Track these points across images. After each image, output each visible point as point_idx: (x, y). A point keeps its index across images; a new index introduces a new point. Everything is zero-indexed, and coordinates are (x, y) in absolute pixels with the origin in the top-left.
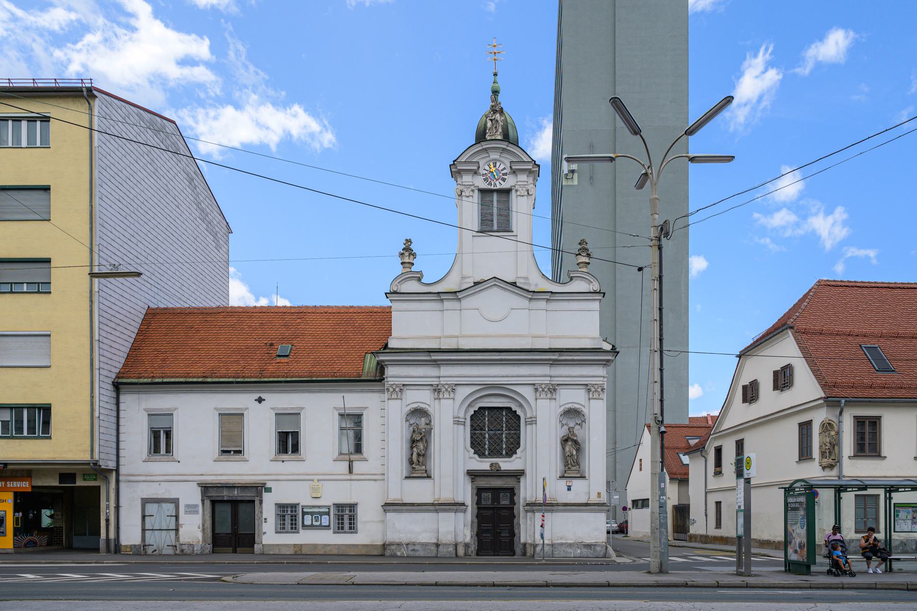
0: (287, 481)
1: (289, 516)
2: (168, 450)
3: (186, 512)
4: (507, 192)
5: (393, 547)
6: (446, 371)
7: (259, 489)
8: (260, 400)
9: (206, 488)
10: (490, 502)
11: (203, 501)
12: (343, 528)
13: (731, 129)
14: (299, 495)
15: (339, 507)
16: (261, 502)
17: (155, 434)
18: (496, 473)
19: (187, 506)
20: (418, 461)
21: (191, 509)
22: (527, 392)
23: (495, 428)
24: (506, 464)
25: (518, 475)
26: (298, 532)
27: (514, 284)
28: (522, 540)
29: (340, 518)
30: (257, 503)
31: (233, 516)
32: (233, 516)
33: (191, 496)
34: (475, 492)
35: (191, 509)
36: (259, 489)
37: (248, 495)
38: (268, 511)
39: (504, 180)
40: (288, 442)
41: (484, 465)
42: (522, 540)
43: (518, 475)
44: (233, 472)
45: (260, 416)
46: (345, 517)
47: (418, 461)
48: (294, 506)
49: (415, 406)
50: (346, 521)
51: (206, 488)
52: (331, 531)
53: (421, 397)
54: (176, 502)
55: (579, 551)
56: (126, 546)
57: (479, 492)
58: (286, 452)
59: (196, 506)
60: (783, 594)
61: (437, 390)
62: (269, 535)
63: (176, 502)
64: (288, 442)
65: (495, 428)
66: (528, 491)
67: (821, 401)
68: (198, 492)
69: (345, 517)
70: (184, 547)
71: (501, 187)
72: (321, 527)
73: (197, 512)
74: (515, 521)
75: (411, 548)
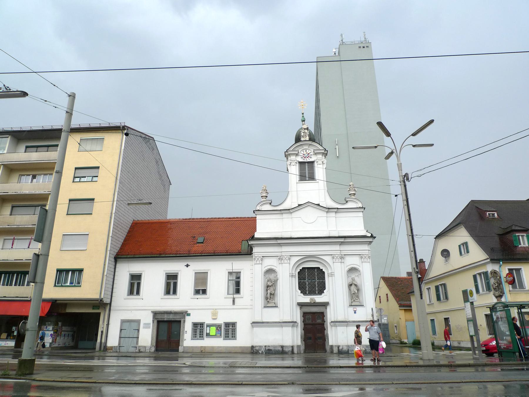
1: (199, 329)
4: (313, 162)
6: (285, 249)
7: (185, 314)
8: (187, 266)
9: (155, 314)
11: (153, 321)
12: (228, 337)
15: (227, 325)
16: (184, 321)
19: (145, 324)
20: (270, 297)
21: (146, 326)
22: (328, 259)
24: (319, 299)
27: (318, 205)
28: (330, 344)
29: (227, 331)
30: (182, 322)
33: (147, 319)
34: (302, 315)
35: (146, 326)
36: (185, 314)
37: (177, 318)
39: (311, 157)
41: (307, 299)
42: (330, 344)
43: (325, 305)
44: (171, 304)
46: (229, 330)
47: (270, 297)
48: (202, 324)
49: (269, 267)
51: (155, 314)
52: (222, 338)
53: (270, 263)
54: (138, 322)
59: (149, 324)
61: (280, 258)
62: (188, 341)
63: (138, 322)
66: (331, 315)
68: (151, 316)
69: (229, 330)
73: (149, 327)
74: (326, 332)
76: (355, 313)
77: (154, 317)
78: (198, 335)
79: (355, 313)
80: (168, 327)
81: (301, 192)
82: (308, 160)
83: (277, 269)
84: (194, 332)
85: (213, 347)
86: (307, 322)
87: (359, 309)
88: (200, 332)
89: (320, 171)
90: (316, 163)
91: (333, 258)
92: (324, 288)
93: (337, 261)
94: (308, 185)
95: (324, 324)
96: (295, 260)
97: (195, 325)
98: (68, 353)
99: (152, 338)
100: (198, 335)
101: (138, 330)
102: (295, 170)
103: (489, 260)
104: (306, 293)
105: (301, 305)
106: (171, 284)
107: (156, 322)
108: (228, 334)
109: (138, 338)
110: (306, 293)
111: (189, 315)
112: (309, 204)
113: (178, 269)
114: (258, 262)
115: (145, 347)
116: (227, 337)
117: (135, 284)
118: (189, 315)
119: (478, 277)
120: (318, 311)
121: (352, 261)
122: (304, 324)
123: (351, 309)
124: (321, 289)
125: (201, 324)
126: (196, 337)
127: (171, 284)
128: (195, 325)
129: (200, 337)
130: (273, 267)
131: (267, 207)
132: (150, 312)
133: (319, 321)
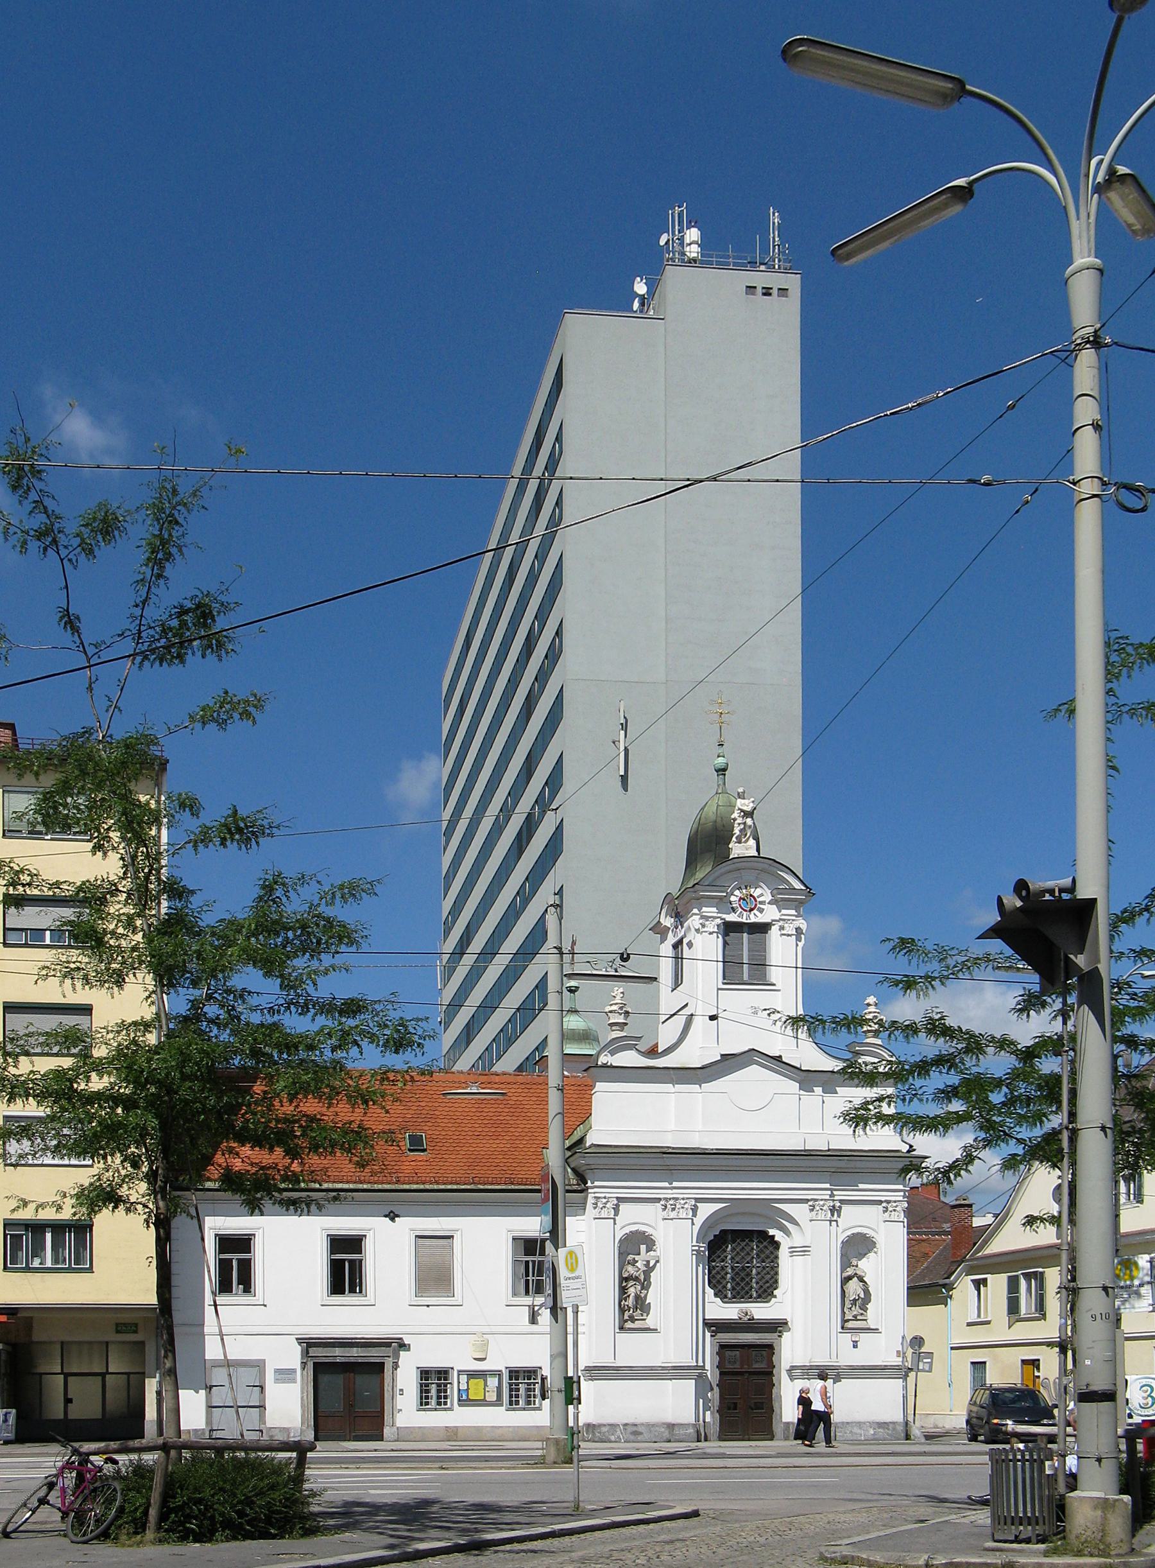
0: (433, 1336)
1: (434, 1383)
3: (277, 1381)
4: (764, 928)
5: (604, 1429)
9: (309, 1344)
12: (517, 1403)
13: (1127, 1019)
14: (456, 1357)
15: (514, 1373)
16: (396, 1366)
19: (277, 1371)
20: (631, 1308)
21: (284, 1375)
23: (740, 1255)
24: (760, 1311)
25: (777, 1327)
26: (451, 1409)
27: (778, 1059)
28: (784, 1420)
34: (717, 1349)
35: (284, 1375)
38: (404, 1380)
39: (761, 911)
41: (730, 1311)
42: (784, 1420)
43: (777, 1327)
44: (348, 1319)
45: (389, 1244)
47: (631, 1308)
48: (443, 1374)
49: (634, 1228)
50: (433, 1392)
51: (309, 1344)
52: (503, 1408)
53: (634, 1217)
56: (189, 1431)
57: (723, 1349)
59: (294, 1371)
60: (1040, 131)
62: (406, 1410)
65: (740, 1255)
66: (792, 1351)
70: (274, 1432)
71: (757, 920)
72: (483, 1403)
73: (294, 1381)
74: (774, 1391)
75: (630, 1429)
76: (855, 1346)
77: (306, 1353)
78: (433, 1402)
79: (855, 1346)
80: (348, 1383)
82: (753, 920)
84: (424, 1391)
86: (729, 1367)
90: (774, 930)
93: (821, 1215)
94: (741, 1001)
95: (771, 1374)
96: (706, 1211)
98: (501, 1468)
99: (302, 1406)
100: (433, 1402)
101: (262, 1388)
104: (726, 1297)
106: (345, 1270)
108: (517, 1396)
109: (262, 1407)
110: (726, 1297)
112: (749, 1057)
114: (604, 1214)
115: (287, 1430)
116: (513, 1403)
118: (403, 1346)
119: (1023, 1283)
120: (758, 1342)
121: (855, 1219)
123: (847, 1338)
124: (767, 1291)
125: (439, 1372)
127: (345, 1270)
128: (424, 1374)
129: (439, 1404)
130: (642, 1228)
131: (629, 1058)
133: (760, 1366)
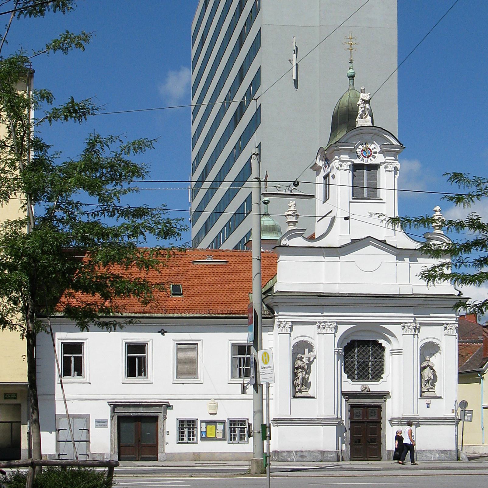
0: (186, 401)
1: (187, 428)
2: (145, 375)
4: (376, 167)
5: (284, 454)
9: (115, 406)
10: (361, 418)
11: (112, 417)
12: (234, 439)
14: (199, 413)
15: (233, 422)
16: (165, 418)
17: (131, 362)
18: (369, 395)
19: (97, 421)
20: (300, 385)
21: (101, 423)
23: (362, 354)
24: (374, 387)
25: (383, 395)
26: (196, 443)
27: (384, 242)
29: (232, 432)
31: (138, 429)
32: (138, 429)
34: (349, 408)
35: (101, 423)
37: (152, 411)
39: (374, 157)
40: (187, 367)
41: (356, 387)
43: (383, 395)
44: (137, 391)
47: (300, 385)
48: (192, 422)
51: (115, 406)
53: (302, 333)
54: (86, 418)
55: (438, 456)
56: (46, 455)
58: (134, 375)
59: (106, 421)
62: (170, 443)
63: (86, 418)
64: (187, 367)
65: (362, 354)
66: (392, 409)
67: (265, 451)
68: (109, 409)
70: (95, 456)
75: (299, 454)
76: (428, 407)
77: (113, 411)
79: (428, 407)
81: (343, 214)
82: (369, 162)
83: (315, 343)
84: (181, 433)
85: (212, 454)
86: (356, 418)
87: (433, 402)
88: (189, 432)
89: (386, 180)
91: (446, 329)
92: (382, 371)
96: (343, 329)
97: (182, 422)
100: (186, 439)
101: (88, 430)
102: (342, 177)
103: (265, 422)
104: (354, 378)
105: (348, 395)
107: (116, 417)
108: (234, 435)
109: (88, 441)
110: (354, 378)
111: (169, 406)
113: (149, 338)
117: (73, 361)
118: (169, 406)
121: (429, 334)
122: (351, 422)
123: (424, 402)
124: (377, 375)
125: (190, 421)
126: (183, 439)
128: (182, 422)
129: (190, 439)
132: (105, 403)
133: (374, 418)
